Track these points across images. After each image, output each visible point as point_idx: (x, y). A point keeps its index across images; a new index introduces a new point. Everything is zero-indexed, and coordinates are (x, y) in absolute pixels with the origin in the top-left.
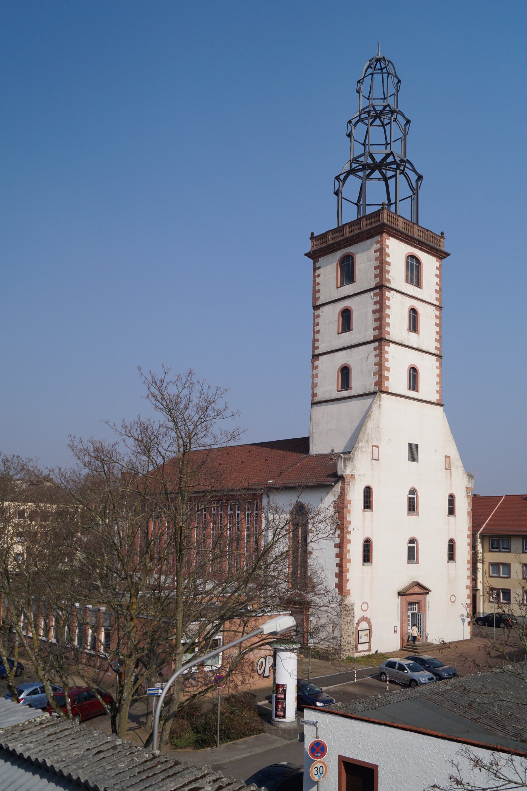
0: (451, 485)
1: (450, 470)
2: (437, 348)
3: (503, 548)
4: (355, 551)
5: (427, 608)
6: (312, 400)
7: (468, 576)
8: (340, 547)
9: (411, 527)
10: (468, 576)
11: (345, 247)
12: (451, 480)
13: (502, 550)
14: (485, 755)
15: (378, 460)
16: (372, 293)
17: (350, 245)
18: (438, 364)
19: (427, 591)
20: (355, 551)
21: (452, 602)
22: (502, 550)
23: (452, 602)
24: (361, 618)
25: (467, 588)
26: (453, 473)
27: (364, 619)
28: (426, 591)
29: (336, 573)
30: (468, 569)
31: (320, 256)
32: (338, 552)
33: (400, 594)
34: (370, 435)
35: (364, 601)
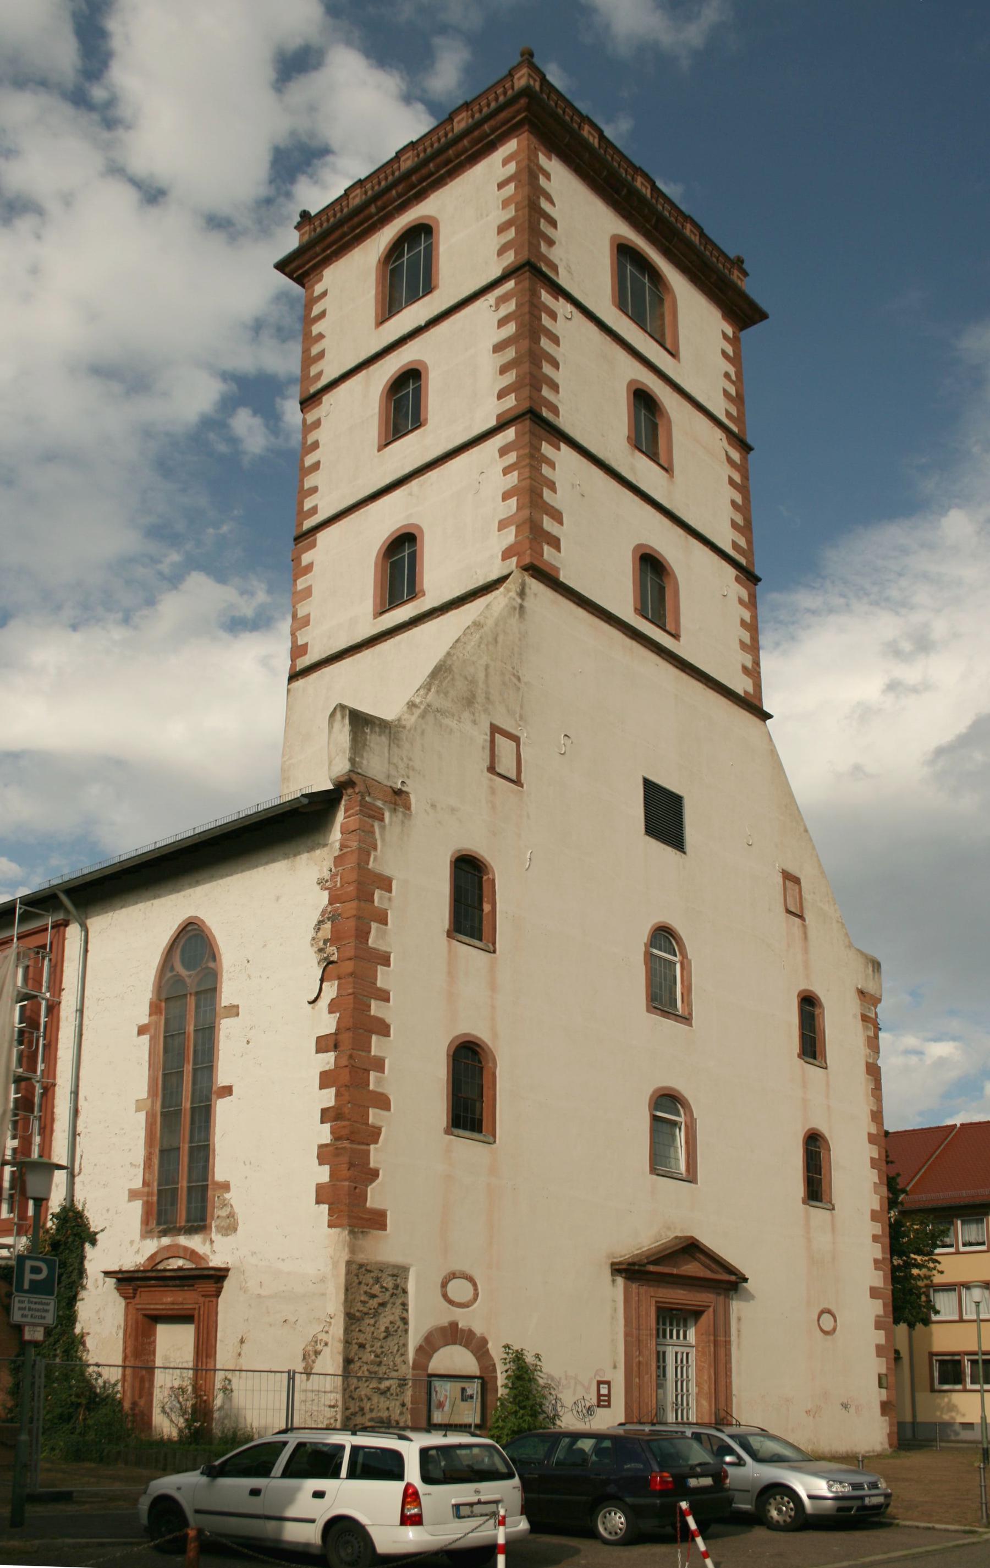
0: (806, 964)
1: (801, 917)
2: (735, 545)
3: (964, 1245)
4: (414, 1079)
5: (734, 1338)
6: (293, 666)
7: (876, 1261)
8: (336, 1047)
9: (660, 1052)
10: (876, 1261)
11: (403, 207)
12: (806, 951)
13: (962, 1249)
14: (330, 1361)
15: (517, 782)
16: (491, 298)
17: (420, 196)
18: (745, 594)
19: (733, 1278)
20: (414, 1079)
21: (826, 1333)
22: (962, 1249)
23: (826, 1333)
24: (442, 1330)
25: (872, 1296)
26: (812, 933)
27: (453, 1334)
28: (729, 1282)
29: (321, 1147)
30: (875, 1238)
31: (327, 261)
32: (331, 1066)
33: (632, 1271)
34: (481, 685)
35: (457, 1267)
